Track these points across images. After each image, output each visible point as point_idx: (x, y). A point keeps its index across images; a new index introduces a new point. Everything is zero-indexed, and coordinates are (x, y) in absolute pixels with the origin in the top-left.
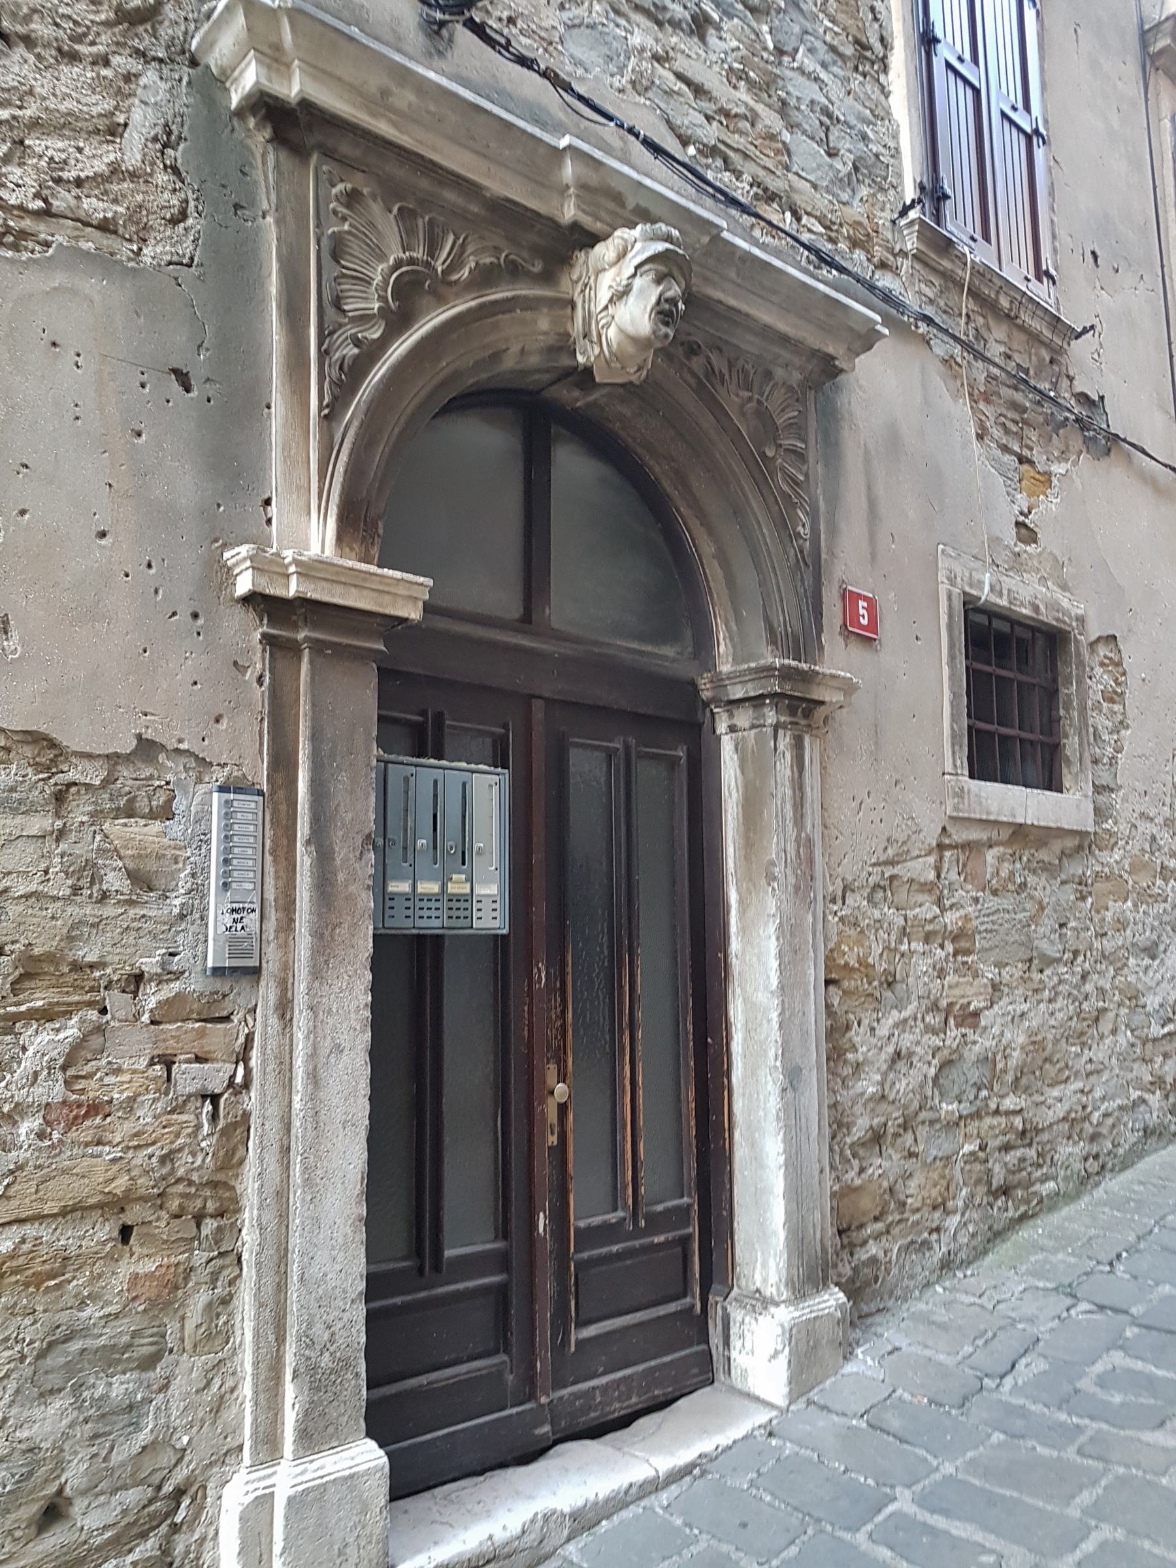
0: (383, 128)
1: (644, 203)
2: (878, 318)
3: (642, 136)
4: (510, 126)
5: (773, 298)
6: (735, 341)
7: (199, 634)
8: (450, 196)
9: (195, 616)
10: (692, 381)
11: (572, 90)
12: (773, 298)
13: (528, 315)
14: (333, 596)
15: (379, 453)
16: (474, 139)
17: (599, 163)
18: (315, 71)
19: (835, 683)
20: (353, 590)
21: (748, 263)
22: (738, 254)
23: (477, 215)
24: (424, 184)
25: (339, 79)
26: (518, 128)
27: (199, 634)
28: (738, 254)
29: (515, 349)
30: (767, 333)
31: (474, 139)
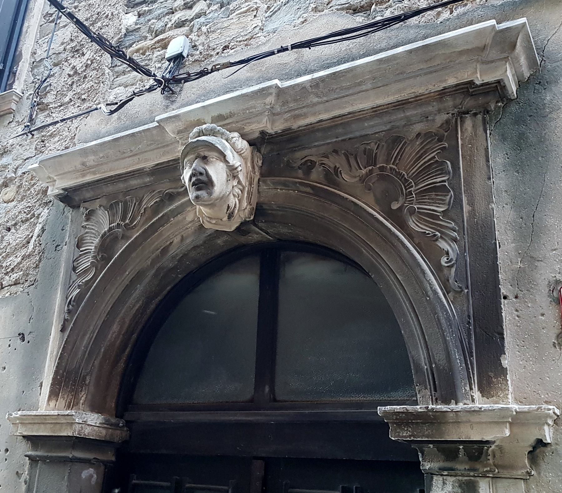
0: (89, 178)
1: (216, 114)
2: (493, 22)
3: (290, 48)
4: (133, 134)
5: (364, 87)
6: (357, 134)
7: (6, 460)
8: (134, 182)
9: (7, 450)
10: (309, 190)
11: (232, 63)
12: (364, 87)
13: (180, 217)
14: (33, 432)
15: (85, 341)
16: (124, 153)
17: (176, 117)
18: (63, 175)
19: (475, 418)
20: (42, 426)
21: (321, 85)
22: (308, 86)
23: (149, 182)
24: (121, 186)
25: (69, 172)
26: (137, 133)
27: (6, 460)
28: (308, 86)
29: (177, 240)
30: (377, 112)
31: (124, 153)
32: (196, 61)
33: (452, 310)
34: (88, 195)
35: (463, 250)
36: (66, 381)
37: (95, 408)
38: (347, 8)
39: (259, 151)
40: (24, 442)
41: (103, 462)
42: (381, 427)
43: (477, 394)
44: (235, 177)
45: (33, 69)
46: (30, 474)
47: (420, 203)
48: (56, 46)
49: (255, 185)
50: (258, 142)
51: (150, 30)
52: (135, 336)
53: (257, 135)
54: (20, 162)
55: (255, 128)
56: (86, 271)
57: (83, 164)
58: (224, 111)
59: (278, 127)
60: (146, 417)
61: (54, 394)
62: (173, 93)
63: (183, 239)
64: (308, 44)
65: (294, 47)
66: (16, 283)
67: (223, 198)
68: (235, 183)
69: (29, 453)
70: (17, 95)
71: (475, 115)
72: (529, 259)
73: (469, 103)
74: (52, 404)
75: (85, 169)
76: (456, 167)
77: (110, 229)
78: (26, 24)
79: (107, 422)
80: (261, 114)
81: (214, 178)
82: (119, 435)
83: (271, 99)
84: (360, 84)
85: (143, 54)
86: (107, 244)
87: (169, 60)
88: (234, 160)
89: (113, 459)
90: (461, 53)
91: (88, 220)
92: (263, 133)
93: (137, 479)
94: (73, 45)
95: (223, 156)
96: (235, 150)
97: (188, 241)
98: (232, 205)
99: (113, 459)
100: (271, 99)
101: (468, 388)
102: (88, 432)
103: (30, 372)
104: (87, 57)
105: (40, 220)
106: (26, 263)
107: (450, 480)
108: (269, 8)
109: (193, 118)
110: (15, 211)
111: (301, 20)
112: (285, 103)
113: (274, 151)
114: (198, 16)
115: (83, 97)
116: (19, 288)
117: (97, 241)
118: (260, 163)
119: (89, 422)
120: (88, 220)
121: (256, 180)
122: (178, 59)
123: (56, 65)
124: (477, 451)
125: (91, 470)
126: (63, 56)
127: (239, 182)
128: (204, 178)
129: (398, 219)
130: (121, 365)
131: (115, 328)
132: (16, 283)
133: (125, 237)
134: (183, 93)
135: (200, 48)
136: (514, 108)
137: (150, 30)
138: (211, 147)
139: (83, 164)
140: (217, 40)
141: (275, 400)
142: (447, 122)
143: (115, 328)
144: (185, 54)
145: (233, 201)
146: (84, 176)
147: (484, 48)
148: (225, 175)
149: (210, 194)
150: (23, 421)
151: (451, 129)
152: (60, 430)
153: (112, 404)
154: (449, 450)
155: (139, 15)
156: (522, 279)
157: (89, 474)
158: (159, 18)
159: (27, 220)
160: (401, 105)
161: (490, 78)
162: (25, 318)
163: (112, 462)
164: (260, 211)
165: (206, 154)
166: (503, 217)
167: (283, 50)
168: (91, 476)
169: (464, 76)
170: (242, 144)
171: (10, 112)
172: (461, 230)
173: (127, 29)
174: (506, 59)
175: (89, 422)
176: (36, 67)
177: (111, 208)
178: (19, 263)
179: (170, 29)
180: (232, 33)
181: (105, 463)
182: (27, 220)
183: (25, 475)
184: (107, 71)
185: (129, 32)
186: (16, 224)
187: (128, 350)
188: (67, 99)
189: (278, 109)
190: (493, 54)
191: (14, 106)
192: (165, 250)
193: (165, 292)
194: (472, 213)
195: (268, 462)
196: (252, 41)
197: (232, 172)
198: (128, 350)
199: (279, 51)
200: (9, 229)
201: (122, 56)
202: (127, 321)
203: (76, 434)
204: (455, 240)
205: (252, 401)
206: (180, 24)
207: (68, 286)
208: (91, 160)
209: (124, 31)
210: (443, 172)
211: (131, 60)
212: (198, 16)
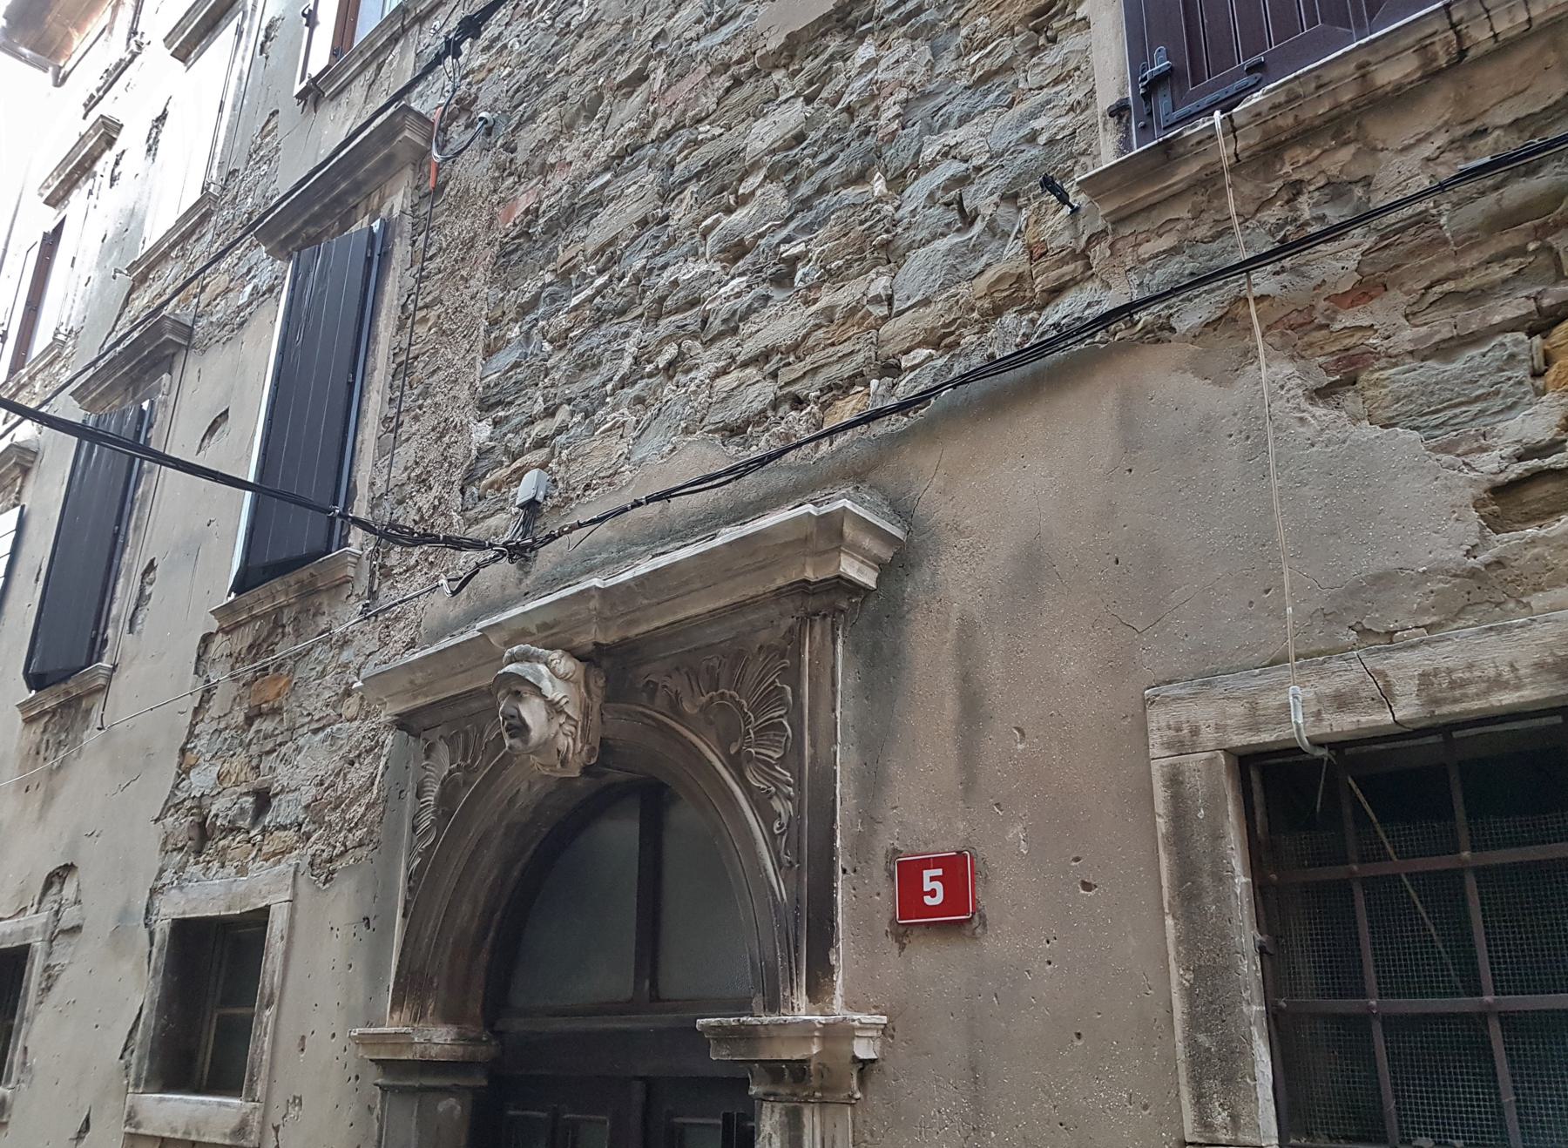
12: (695, 586)
29: (524, 786)
30: (715, 616)
32: (554, 506)
33: (781, 890)
34: (427, 722)
35: (799, 810)
36: (411, 987)
37: (447, 1018)
38: (724, 429)
39: (598, 666)
40: (375, 1067)
41: (467, 1088)
42: (698, 1041)
43: (801, 1000)
44: (561, 712)
45: (372, 509)
46: (382, 1109)
47: (759, 746)
48: (398, 475)
49: (595, 716)
50: (589, 658)
51: (507, 451)
52: (498, 915)
53: (591, 647)
54: (362, 659)
55: (587, 638)
56: (427, 832)
57: (412, 682)
58: (549, 619)
59: (611, 637)
60: (518, 1025)
61: (397, 1004)
62: (527, 559)
63: (530, 787)
64: (666, 495)
65: (649, 500)
66: (360, 845)
67: (547, 744)
68: (562, 719)
69: (379, 1081)
70: (352, 554)
71: (825, 616)
72: (869, 818)
73: (812, 603)
74: (396, 1016)
75: (415, 690)
76: (797, 695)
77: (450, 772)
78: (359, 438)
79: (461, 1036)
80: (589, 621)
81: (529, 721)
82: (483, 1052)
83: (594, 604)
84: (686, 583)
85: (499, 490)
86: (449, 789)
87: (521, 506)
88: (555, 691)
89: (484, 1083)
90: (786, 545)
91: (427, 758)
92: (596, 644)
93: (516, 1108)
94: (418, 471)
95: (537, 691)
96: (554, 677)
97: (536, 788)
98: (563, 749)
99: (484, 1083)
100: (594, 604)
101: (787, 993)
102: (434, 1053)
103: (375, 973)
104: (434, 493)
105: (386, 751)
106: (370, 816)
107: (779, 1106)
108: (638, 422)
109: (517, 626)
110: (358, 736)
111: (670, 447)
112: (613, 606)
113: (612, 666)
114: (559, 432)
115: (431, 559)
116: (364, 851)
117: (437, 788)
118: (601, 683)
119: (439, 1038)
120: (427, 758)
121: (596, 708)
122: (531, 506)
123: (400, 502)
124: (799, 1070)
125: (452, 1101)
126: (408, 488)
127: (569, 717)
128: (515, 722)
129: (736, 764)
130: (484, 957)
131: (465, 908)
132: (360, 845)
133: (467, 784)
134: (539, 558)
135: (560, 485)
136: (872, 604)
137: (507, 451)
138: (522, 680)
139: (412, 682)
140: (579, 474)
141: (658, 999)
142: (791, 630)
143: (465, 908)
144: (539, 499)
145: (564, 742)
146: (415, 697)
147: (806, 540)
148: (544, 713)
149: (526, 742)
150: (362, 1040)
151: (794, 640)
152: (400, 1052)
153: (475, 1009)
154: (775, 1070)
155: (496, 423)
156: (861, 847)
157: (449, 1106)
158: (516, 431)
159: (372, 749)
160: (739, 607)
161: (827, 573)
162: (369, 897)
163: (481, 1087)
164: (606, 748)
165: (519, 688)
166: (844, 761)
167: (637, 504)
168: (452, 1108)
169: (794, 576)
170: (565, 665)
171: (347, 581)
172: (798, 785)
173: (479, 449)
174: (838, 550)
175: (439, 1038)
176: (377, 506)
177: (450, 741)
178: (363, 815)
179: (529, 450)
180: (594, 463)
181: (473, 1090)
182: (372, 749)
183: (377, 1111)
184: (456, 517)
185: (483, 453)
186: (359, 755)
187: (491, 934)
188: (412, 562)
189: (608, 614)
190: (822, 545)
191: (351, 572)
192: (512, 801)
193: (529, 853)
194: (814, 757)
195: (649, 1083)
196: (616, 479)
197: (554, 708)
198: (491, 934)
199: (633, 507)
200: (352, 763)
201: (436, 539)
202: (482, 899)
203: (417, 1057)
204: (789, 798)
205: (630, 1001)
206: (540, 444)
207: (412, 849)
208: (419, 677)
209: (474, 452)
210: (782, 702)
211: (447, 540)
212: (559, 432)
